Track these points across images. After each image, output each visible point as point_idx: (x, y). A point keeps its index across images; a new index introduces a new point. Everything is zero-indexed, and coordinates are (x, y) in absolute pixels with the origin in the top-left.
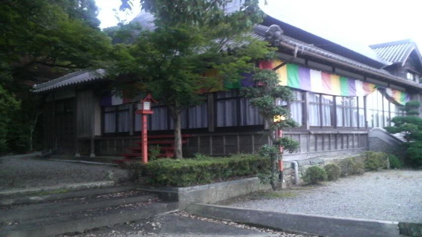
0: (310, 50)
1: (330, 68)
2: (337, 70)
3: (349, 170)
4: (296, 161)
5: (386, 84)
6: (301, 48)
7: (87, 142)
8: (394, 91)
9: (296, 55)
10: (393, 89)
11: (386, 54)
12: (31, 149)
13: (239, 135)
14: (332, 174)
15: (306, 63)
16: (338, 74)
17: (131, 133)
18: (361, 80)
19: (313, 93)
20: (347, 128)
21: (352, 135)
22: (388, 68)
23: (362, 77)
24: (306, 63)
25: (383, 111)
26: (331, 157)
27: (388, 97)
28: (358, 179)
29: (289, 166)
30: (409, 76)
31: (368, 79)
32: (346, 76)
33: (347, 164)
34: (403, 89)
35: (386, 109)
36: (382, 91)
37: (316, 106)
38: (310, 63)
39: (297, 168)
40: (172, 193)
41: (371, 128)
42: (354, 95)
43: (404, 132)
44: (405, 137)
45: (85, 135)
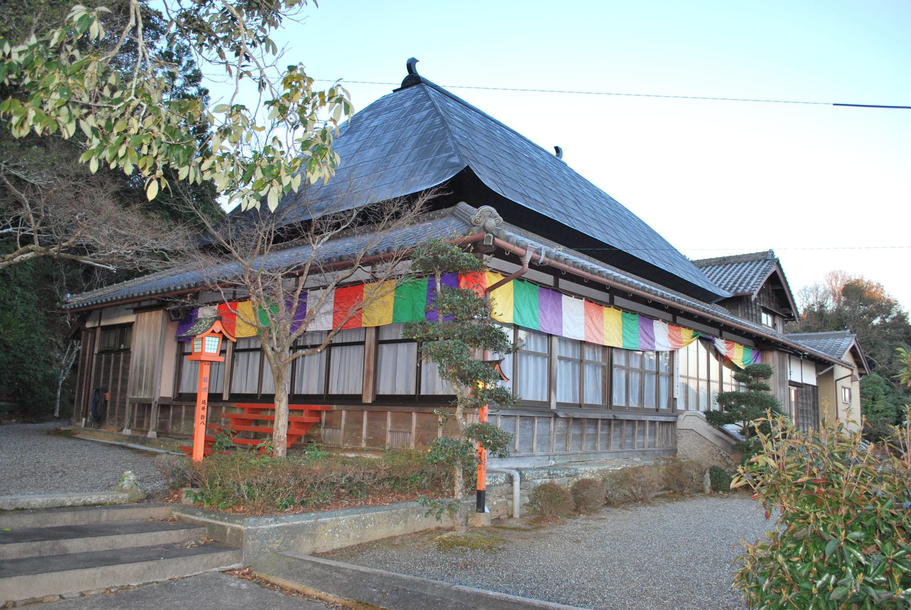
0: (557, 258)
1: (604, 296)
2: (618, 300)
3: (625, 493)
4: (518, 469)
5: (716, 331)
6: (538, 252)
7: (145, 406)
8: (729, 345)
9: (527, 266)
10: (728, 341)
11: (751, 274)
12: (57, 414)
13: (417, 412)
14: (581, 500)
15: (556, 282)
16: (618, 308)
17: (226, 397)
18: (665, 321)
19: (566, 340)
20: (635, 410)
21: (642, 422)
22: (724, 302)
23: (669, 317)
24: (556, 282)
25: (709, 381)
26: (597, 463)
27: (718, 355)
28: (645, 512)
29: (501, 479)
30: (766, 319)
31: (679, 320)
32: (634, 312)
33: (623, 478)
34: (750, 342)
35: (714, 376)
36: (707, 341)
37: (570, 364)
38: (563, 284)
39: (517, 484)
40: (233, 530)
41: (682, 412)
42: (650, 348)
43: (741, 424)
44: (742, 433)
45: (143, 395)
